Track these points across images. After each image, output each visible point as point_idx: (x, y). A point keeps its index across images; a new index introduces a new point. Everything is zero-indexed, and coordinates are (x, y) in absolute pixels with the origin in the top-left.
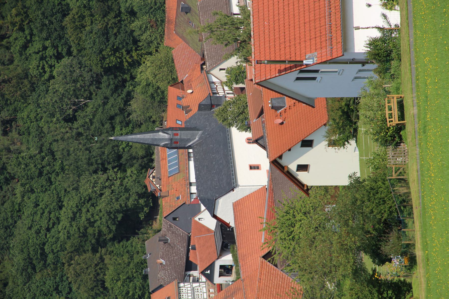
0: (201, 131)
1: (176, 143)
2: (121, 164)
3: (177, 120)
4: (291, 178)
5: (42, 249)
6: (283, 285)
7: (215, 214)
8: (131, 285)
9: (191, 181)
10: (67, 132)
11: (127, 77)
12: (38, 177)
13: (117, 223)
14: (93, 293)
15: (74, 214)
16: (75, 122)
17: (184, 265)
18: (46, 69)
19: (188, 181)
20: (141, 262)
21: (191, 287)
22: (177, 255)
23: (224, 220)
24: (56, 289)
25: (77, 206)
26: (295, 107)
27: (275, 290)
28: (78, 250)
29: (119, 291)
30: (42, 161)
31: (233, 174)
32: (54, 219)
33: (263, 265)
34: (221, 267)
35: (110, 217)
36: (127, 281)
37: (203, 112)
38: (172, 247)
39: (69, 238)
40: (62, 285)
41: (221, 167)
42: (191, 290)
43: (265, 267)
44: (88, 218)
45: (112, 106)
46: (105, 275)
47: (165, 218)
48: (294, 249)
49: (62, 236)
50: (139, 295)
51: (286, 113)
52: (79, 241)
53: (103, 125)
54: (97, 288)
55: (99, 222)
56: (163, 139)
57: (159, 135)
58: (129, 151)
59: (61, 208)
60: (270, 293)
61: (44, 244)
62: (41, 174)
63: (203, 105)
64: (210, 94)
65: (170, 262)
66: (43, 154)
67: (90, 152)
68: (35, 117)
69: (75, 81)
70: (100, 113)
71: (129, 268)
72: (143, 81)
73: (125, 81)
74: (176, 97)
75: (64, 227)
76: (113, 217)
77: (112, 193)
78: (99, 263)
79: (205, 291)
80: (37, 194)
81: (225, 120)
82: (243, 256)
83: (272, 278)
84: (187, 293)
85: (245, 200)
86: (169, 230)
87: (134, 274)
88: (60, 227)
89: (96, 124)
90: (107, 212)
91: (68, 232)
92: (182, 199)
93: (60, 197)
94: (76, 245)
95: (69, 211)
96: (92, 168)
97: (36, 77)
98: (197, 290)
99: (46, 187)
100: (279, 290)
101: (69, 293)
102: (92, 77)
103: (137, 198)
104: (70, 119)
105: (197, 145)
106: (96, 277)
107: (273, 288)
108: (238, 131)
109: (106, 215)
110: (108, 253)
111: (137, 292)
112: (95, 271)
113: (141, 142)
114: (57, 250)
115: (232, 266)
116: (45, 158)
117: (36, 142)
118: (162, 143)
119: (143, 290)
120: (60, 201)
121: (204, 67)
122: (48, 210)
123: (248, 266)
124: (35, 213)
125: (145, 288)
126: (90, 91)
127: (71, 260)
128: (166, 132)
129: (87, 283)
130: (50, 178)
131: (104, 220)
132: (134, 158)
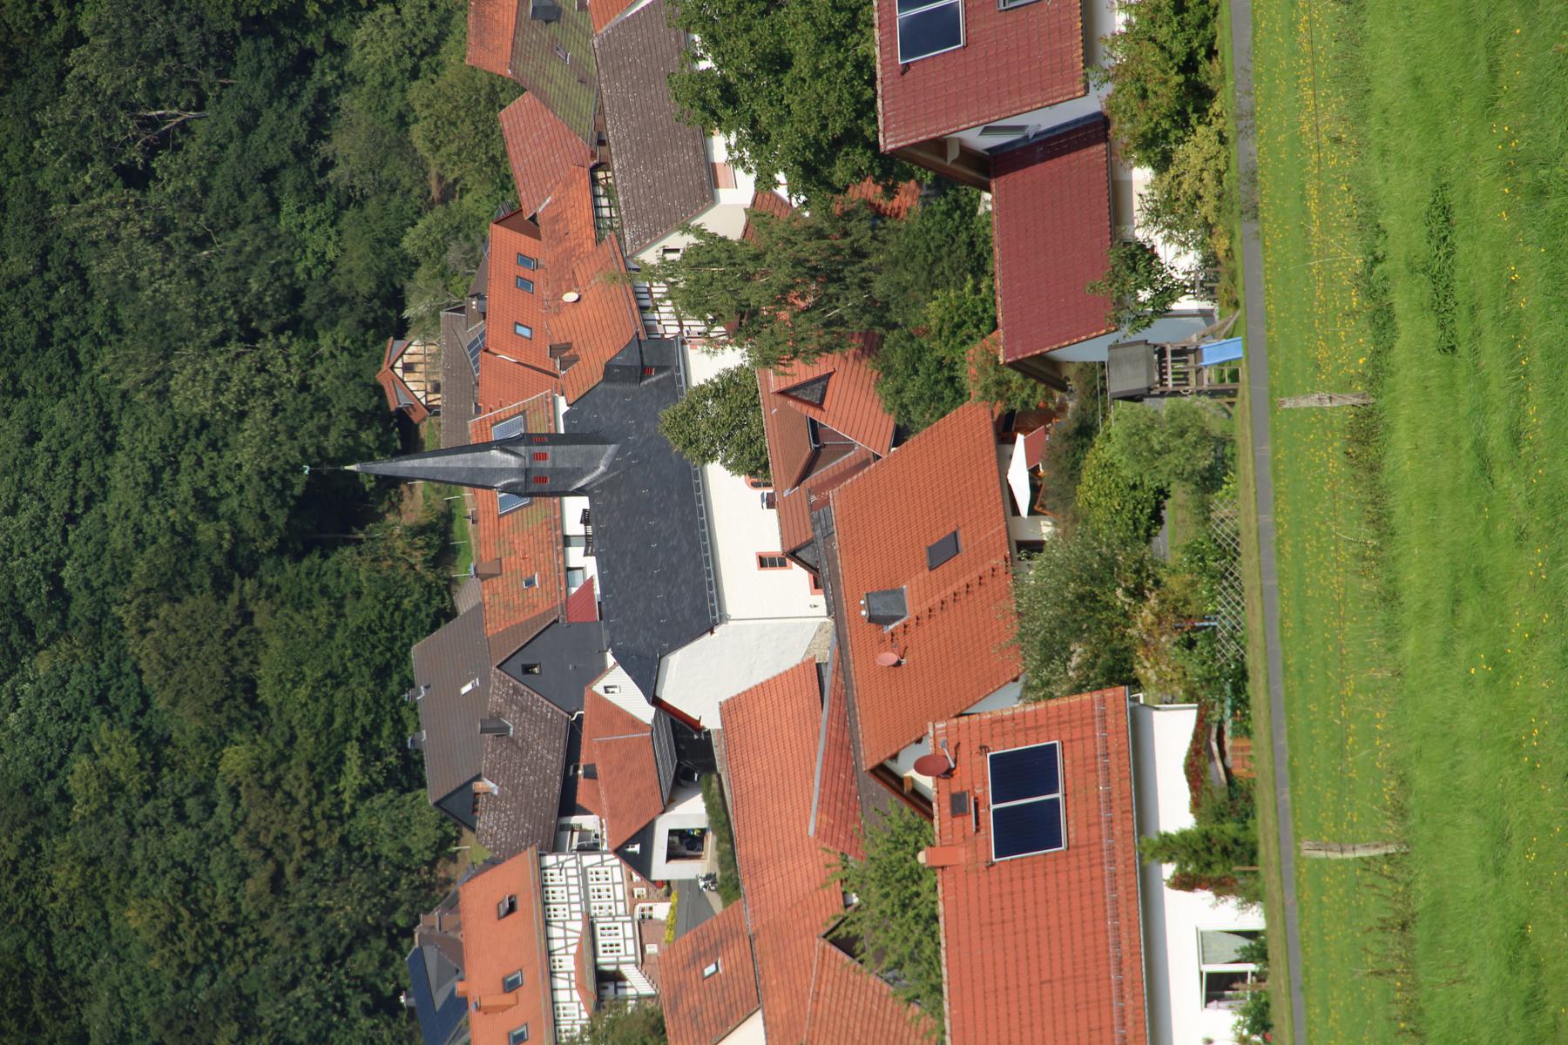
0: (613, 446)
1: (543, 480)
2: (301, 319)
3: (516, 323)
4: (917, 801)
5: (56, 580)
6: (881, 1014)
7: (658, 694)
8: (339, 695)
9: (568, 532)
10: (127, 220)
11: (313, 40)
12: (35, 349)
13: (292, 503)
14: (221, 719)
15: (156, 472)
16: (151, 184)
17: (556, 801)
18: (56, 11)
19: (559, 532)
20: (369, 627)
21: (576, 868)
22: (534, 772)
23: (685, 711)
24: (102, 700)
25: (164, 448)
26: (933, 620)
27: (858, 1025)
28: (171, 586)
29: (304, 716)
30: (48, 298)
31: (710, 583)
32: (92, 484)
33: (827, 958)
34: (672, 832)
35: (270, 486)
36: (325, 685)
37: (617, 387)
38: (521, 749)
39: (140, 545)
40: (119, 688)
41: (674, 560)
42: (578, 876)
43: (832, 965)
44: (199, 485)
45: (272, 137)
46: (255, 662)
47: (498, 667)
48: (918, 944)
49: (119, 539)
50: (363, 727)
51: (908, 637)
52: (174, 559)
53: (242, 197)
54: (231, 701)
55: (234, 502)
56: (502, 469)
57: (491, 458)
58: (325, 278)
59: (110, 448)
60: (844, 1031)
61: (60, 564)
62: (44, 340)
63: (619, 367)
64: (638, 334)
65: (514, 789)
66: (50, 276)
67: (202, 283)
68: (23, 160)
69: (152, 58)
70: (233, 159)
71: (333, 644)
72: (372, 71)
73: (309, 55)
74: (514, 256)
75: (123, 513)
76: (278, 486)
77: (274, 414)
78: (236, 629)
79: (618, 878)
80: (32, 401)
81: (691, 443)
82: (751, 863)
83: (849, 993)
84: (569, 903)
85: (755, 698)
86: (512, 701)
87: (349, 665)
88: (109, 508)
89: (221, 191)
90: (260, 473)
91: (138, 530)
92: (541, 585)
93: (108, 415)
94: (163, 570)
95: (138, 464)
96: (207, 335)
97: (25, 35)
98: (594, 876)
99: (63, 380)
100: (872, 1026)
101: (141, 713)
102: (205, 43)
103: (353, 426)
104: (137, 178)
105: (601, 486)
106: (227, 671)
107: (852, 1020)
108: (728, 473)
109: (255, 479)
110: (263, 594)
111: (357, 719)
112: (226, 652)
113: (439, 477)
114: (101, 580)
115: (703, 831)
116: (57, 289)
117: (27, 238)
118: (500, 480)
119: (377, 713)
120: (107, 424)
121: (601, 175)
122: (69, 452)
123: (769, 893)
124: (28, 462)
125: (383, 708)
126: (197, 85)
127: (147, 618)
128: (510, 448)
129: (201, 687)
130: (73, 354)
131: (250, 494)
132: (342, 300)
